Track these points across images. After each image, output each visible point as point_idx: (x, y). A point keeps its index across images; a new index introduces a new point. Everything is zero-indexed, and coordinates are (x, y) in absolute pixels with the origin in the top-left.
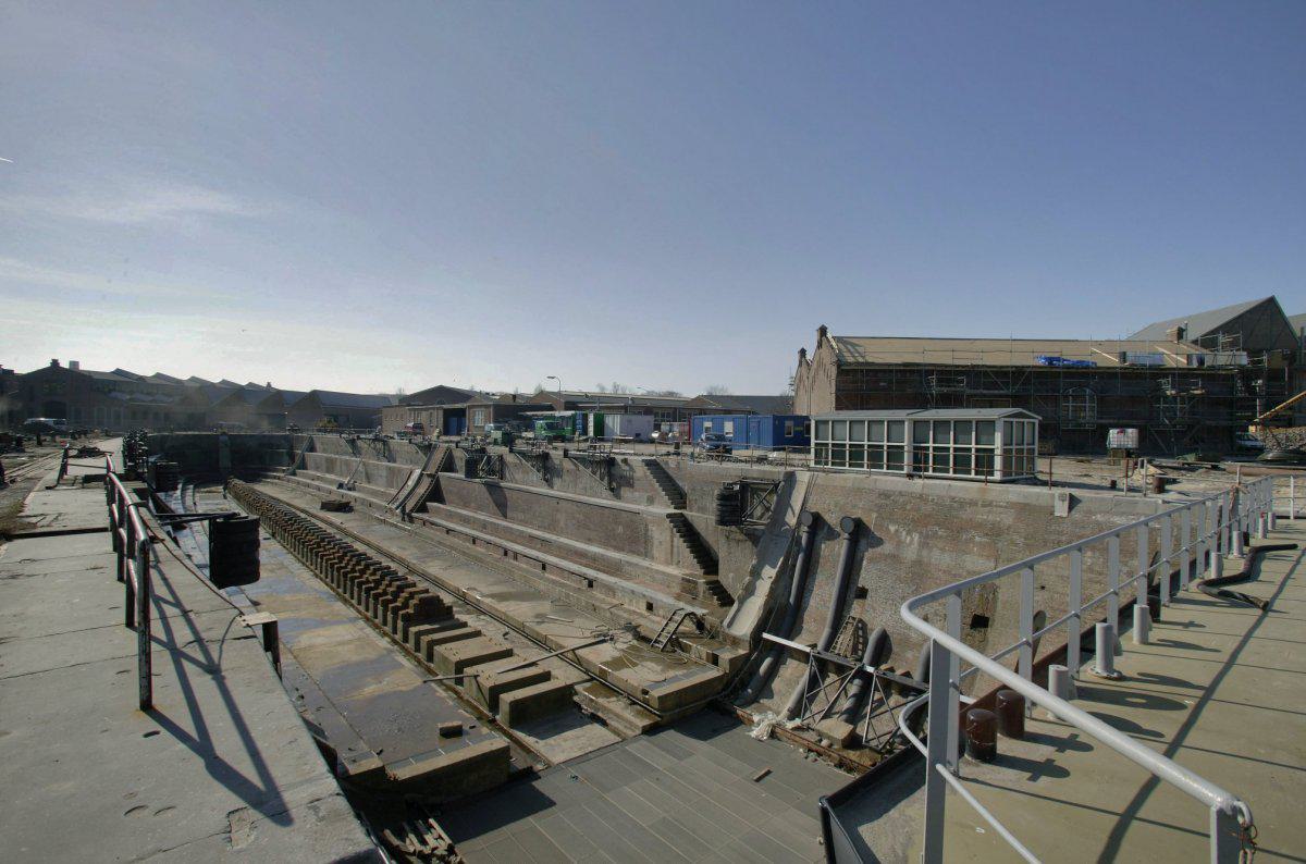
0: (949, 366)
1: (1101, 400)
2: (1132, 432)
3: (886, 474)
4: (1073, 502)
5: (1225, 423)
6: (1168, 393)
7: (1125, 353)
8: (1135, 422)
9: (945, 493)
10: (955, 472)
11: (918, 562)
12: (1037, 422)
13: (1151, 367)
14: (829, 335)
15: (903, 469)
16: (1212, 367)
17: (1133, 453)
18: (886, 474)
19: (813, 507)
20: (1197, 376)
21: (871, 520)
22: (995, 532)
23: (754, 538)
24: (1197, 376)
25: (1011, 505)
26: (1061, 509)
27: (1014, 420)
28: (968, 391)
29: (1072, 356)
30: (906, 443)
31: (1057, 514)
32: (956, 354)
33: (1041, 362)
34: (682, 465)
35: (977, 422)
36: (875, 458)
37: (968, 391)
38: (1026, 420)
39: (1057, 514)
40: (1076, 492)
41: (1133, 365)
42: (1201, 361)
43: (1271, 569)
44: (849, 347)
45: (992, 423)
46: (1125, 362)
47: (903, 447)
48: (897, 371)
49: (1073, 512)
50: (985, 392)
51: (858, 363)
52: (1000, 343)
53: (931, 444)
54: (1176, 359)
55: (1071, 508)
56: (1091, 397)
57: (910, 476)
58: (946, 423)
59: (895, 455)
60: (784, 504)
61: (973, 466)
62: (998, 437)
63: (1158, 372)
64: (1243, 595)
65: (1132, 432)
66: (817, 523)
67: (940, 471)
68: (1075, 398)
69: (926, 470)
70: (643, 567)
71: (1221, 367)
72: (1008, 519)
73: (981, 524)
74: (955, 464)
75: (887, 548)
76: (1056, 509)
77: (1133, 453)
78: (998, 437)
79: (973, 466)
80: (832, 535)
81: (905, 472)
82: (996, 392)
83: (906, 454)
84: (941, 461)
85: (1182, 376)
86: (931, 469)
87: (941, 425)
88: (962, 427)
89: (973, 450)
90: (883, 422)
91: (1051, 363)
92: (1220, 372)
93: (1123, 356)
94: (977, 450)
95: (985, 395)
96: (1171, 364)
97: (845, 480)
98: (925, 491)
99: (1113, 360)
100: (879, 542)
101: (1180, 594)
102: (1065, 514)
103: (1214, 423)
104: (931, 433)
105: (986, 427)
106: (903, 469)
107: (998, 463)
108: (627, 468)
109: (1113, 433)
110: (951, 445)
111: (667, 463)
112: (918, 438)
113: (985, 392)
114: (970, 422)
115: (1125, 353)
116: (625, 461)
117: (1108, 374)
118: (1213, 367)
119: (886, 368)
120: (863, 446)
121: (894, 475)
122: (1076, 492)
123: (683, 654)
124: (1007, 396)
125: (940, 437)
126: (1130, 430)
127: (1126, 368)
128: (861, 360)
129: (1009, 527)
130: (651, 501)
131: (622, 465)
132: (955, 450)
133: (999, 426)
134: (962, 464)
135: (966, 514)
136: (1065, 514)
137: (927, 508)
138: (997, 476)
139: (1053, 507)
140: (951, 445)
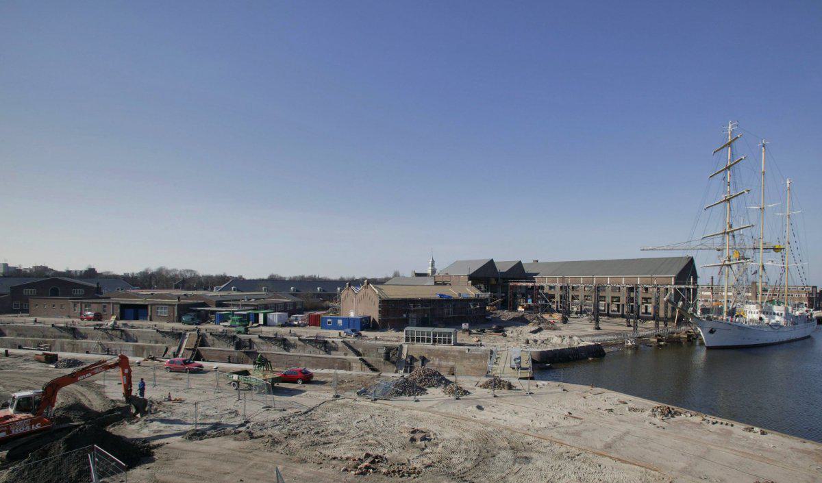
2: (467, 324)
11: (439, 364)
19: (410, 353)
21: (426, 356)
22: (455, 357)
23: (393, 363)
25: (457, 351)
26: (467, 351)
30: (431, 337)
36: (423, 340)
42: (480, 296)
43: (498, 360)
59: (429, 341)
60: (401, 354)
65: (467, 324)
66: (412, 358)
70: (11, 422)
72: (457, 354)
75: (431, 362)
80: (416, 360)
84: (440, 342)
87: (440, 334)
93: (460, 295)
100: (429, 361)
101: (429, 272)
107: (452, 342)
112: (434, 335)
116: (333, 342)
117: (456, 300)
123: (705, 274)
130: (346, 354)
131: (333, 344)
134: (444, 342)
135: (449, 353)
137: (439, 353)
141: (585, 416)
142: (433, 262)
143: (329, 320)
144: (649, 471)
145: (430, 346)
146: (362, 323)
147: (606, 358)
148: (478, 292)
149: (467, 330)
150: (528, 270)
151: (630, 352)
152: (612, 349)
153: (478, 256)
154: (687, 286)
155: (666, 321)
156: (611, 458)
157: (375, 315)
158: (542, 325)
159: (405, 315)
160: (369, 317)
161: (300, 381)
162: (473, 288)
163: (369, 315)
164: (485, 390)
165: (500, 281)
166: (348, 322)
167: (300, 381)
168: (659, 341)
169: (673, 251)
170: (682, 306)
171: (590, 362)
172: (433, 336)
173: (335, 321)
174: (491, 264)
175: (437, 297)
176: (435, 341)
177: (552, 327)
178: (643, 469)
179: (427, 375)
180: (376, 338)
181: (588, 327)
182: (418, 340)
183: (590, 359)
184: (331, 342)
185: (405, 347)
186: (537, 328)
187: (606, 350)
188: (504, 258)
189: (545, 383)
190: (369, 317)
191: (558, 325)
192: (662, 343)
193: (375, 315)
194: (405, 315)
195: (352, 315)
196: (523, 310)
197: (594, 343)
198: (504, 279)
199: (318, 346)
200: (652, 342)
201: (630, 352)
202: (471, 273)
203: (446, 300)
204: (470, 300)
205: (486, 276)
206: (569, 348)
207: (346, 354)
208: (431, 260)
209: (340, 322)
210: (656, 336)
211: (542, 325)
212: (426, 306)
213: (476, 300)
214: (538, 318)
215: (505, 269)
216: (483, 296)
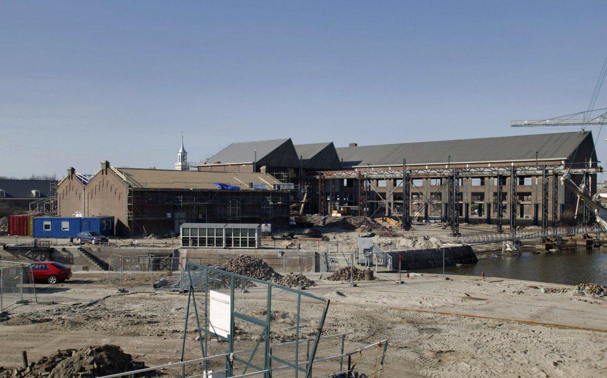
3: (215, 248)
4: (283, 253)
6: (270, 203)
14: (112, 167)
15: (222, 246)
18: (215, 248)
30: (224, 237)
34: (101, 250)
36: (211, 242)
40: (283, 250)
42: (279, 188)
47: (222, 238)
53: (233, 237)
55: (282, 255)
57: (225, 248)
59: (219, 242)
62: (256, 234)
67: (211, 246)
69: (231, 246)
74: (216, 243)
78: (256, 234)
81: (224, 247)
83: (224, 241)
87: (236, 231)
88: (244, 231)
89: (240, 239)
90: (214, 229)
91: (223, 188)
93: (251, 185)
94: (249, 239)
97: (204, 251)
106: (222, 246)
108: (66, 254)
111: (90, 249)
112: (228, 234)
114: (239, 229)
116: (64, 250)
117: (246, 193)
120: (197, 238)
121: (219, 248)
122: (283, 250)
128: (140, 187)
131: (65, 254)
132: (242, 239)
134: (244, 243)
138: (224, 247)
141: (489, 297)
142: (184, 154)
143: (46, 223)
144: (598, 333)
145: (222, 251)
146: (102, 226)
147: (478, 263)
148: (277, 182)
149: (269, 234)
150: (343, 157)
151: (509, 259)
152: (484, 256)
153: (271, 136)
154: (585, 170)
155: (554, 225)
156: (544, 325)
157: (121, 213)
158: (374, 231)
159: (169, 215)
160: (113, 218)
161: (53, 280)
162: (269, 176)
163: (111, 215)
164: (335, 282)
165: (302, 173)
166: (78, 225)
167: (53, 280)
168: (548, 247)
169: (559, 127)
170: (585, 189)
171: (457, 268)
172: (227, 235)
173: (57, 222)
174: (288, 146)
175: (218, 187)
176: (229, 242)
177: (390, 233)
178: (590, 332)
179: (249, 266)
180: (132, 245)
181: (442, 234)
182: (202, 242)
183: (458, 265)
184: (60, 250)
185: (184, 252)
186: (369, 233)
187: (478, 257)
188: (308, 140)
189: (419, 274)
190: (113, 218)
191: (399, 232)
192: (553, 250)
193: (121, 213)
194: (169, 215)
195: (79, 215)
196: (339, 215)
197: (461, 245)
198: (307, 170)
199: (38, 258)
200: (538, 249)
201: (509, 259)
202: (258, 160)
203: (231, 193)
204: (265, 193)
205: (281, 159)
206: (428, 250)
207: (86, 268)
208: (181, 151)
209: (65, 225)
210: (544, 241)
211: (374, 231)
212: (201, 200)
213: (275, 194)
214: (368, 222)
215: (308, 156)
216: (286, 187)
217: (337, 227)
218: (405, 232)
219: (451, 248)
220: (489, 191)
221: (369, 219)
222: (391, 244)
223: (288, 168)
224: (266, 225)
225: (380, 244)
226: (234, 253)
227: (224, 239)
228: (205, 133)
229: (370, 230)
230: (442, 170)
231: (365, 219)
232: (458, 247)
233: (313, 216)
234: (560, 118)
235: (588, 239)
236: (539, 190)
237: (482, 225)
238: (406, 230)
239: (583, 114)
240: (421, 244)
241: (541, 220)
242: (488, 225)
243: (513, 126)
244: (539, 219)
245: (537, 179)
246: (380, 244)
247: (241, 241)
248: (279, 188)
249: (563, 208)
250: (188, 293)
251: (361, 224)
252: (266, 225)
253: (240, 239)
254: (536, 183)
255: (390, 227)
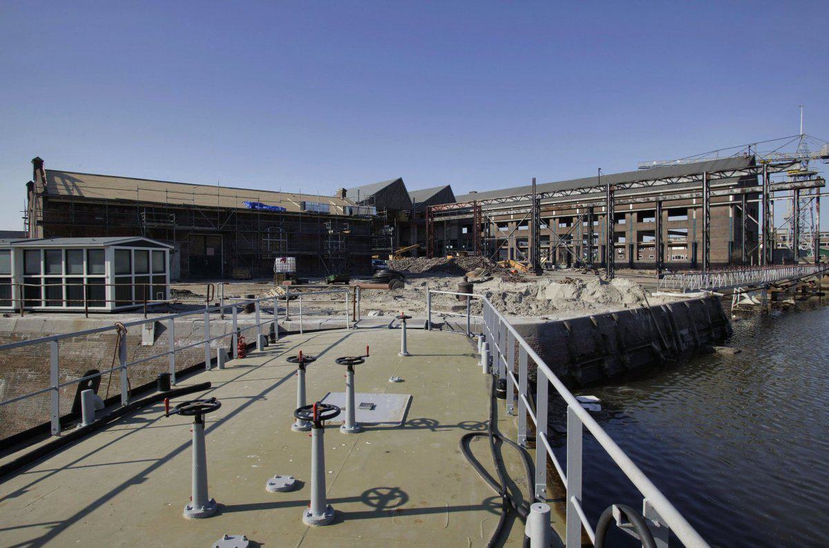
0: (163, 204)
1: (290, 237)
4: (159, 329)
5: (365, 254)
7: (305, 202)
8: (292, 253)
9: (39, 331)
10: (68, 305)
12: (167, 251)
13: (322, 214)
16: (357, 216)
17: (291, 276)
20: (347, 221)
24: (347, 221)
26: (147, 338)
27: (133, 248)
28: (177, 227)
29: (269, 202)
31: (144, 343)
32: (170, 195)
33: (247, 206)
35: (88, 251)
37: (177, 227)
38: (151, 249)
39: (144, 343)
41: (310, 212)
44: (68, 182)
45: (101, 251)
46: (305, 209)
48: (110, 206)
49: (158, 340)
50: (197, 228)
51: (71, 197)
52: (252, 192)
54: (337, 210)
55: (156, 336)
56: (283, 234)
57: (113, 312)
58: (80, 250)
61: (64, 298)
62: (108, 266)
63: (326, 217)
64: (25, 492)
68: (273, 235)
69: (39, 304)
71: (362, 217)
73: (73, 361)
74: (68, 297)
76: (143, 338)
77: (291, 276)
78: (108, 266)
79: (64, 298)
81: (109, 307)
82: (206, 228)
84: (53, 295)
85: (338, 221)
86: (43, 303)
88: (72, 255)
89: (64, 281)
90: (40, 250)
92: (363, 220)
93: (304, 205)
95: (196, 231)
96: (333, 212)
98: (19, 329)
99: (295, 207)
102: (151, 343)
103: (358, 254)
104: (42, 263)
105: (95, 256)
107: (109, 293)
109: (278, 260)
110: (64, 276)
113: (197, 228)
115: (305, 202)
118: (357, 215)
119: (101, 203)
120: (60, 279)
124: (217, 232)
125: (52, 267)
126: (289, 259)
127: (305, 214)
128: (76, 193)
129: (100, 362)
132: (68, 280)
133: (110, 254)
134: (74, 295)
136: (151, 343)
138: (109, 307)
139: (141, 336)
140: (64, 276)
176: (31, 295)
191: (528, 277)
214: (486, 264)
217: (443, 271)
218: (537, 277)
219: (689, 302)
220: (631, 230)
221: (487, 260)
222: (527, 293)
223: (398, 210)
224: (283, 260)
225: (504, 295)
226: (11, 329)
227: (108, 281)
228: (321, 174)
229: (488, 275)
230: (588, 189)
231: (482, 260)
232: (695, 303)
233: (418, 260)
234: (693, 158)
235: (773, 289)
236: (697, 225)
237: (625, 270)
238: (537, 275)
239: (716, 153)
240: (593, 294)
241: (701, 262)
242: (632, 270)
243: (404, 381)
244: (698, 262)
245: (694, 212)
246: (504, 295)
247: (47, 288)
248: (351, 212)
249: (732, 246)
250: (467, 309)
251: (477, 266)
252: (283, 260)
253: (64, 281)
254: (694, 217)
255: (516, 271)
